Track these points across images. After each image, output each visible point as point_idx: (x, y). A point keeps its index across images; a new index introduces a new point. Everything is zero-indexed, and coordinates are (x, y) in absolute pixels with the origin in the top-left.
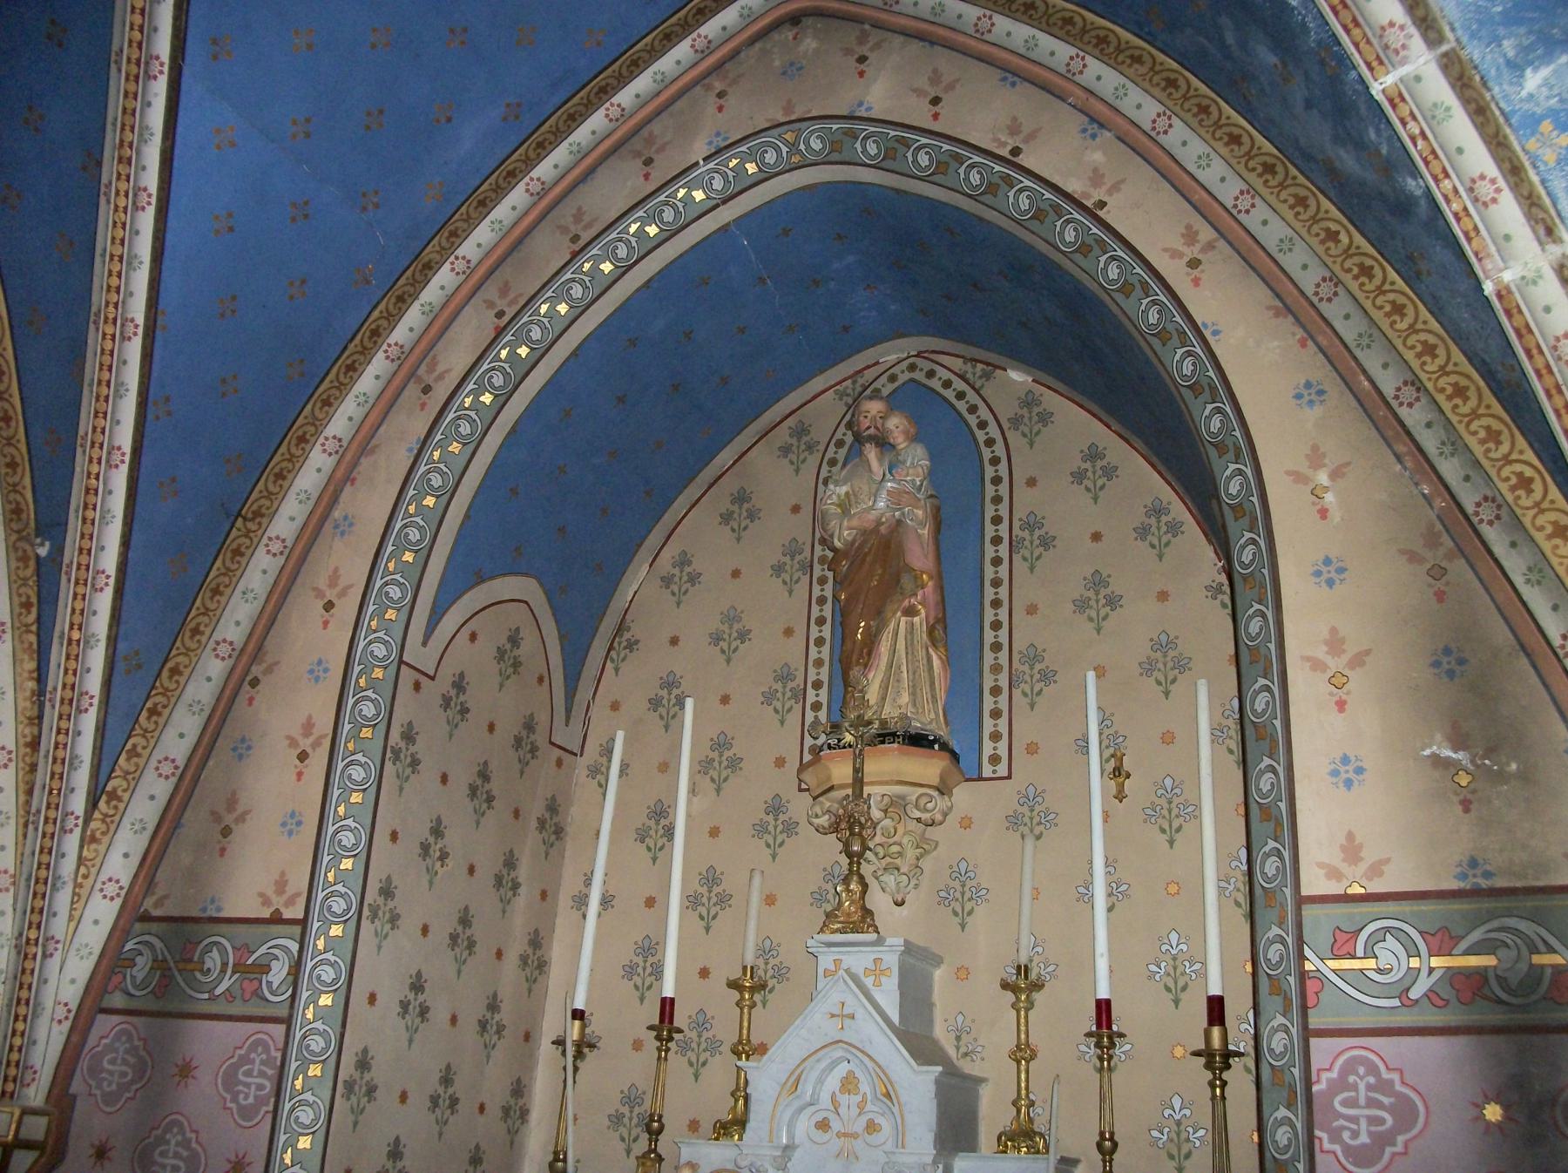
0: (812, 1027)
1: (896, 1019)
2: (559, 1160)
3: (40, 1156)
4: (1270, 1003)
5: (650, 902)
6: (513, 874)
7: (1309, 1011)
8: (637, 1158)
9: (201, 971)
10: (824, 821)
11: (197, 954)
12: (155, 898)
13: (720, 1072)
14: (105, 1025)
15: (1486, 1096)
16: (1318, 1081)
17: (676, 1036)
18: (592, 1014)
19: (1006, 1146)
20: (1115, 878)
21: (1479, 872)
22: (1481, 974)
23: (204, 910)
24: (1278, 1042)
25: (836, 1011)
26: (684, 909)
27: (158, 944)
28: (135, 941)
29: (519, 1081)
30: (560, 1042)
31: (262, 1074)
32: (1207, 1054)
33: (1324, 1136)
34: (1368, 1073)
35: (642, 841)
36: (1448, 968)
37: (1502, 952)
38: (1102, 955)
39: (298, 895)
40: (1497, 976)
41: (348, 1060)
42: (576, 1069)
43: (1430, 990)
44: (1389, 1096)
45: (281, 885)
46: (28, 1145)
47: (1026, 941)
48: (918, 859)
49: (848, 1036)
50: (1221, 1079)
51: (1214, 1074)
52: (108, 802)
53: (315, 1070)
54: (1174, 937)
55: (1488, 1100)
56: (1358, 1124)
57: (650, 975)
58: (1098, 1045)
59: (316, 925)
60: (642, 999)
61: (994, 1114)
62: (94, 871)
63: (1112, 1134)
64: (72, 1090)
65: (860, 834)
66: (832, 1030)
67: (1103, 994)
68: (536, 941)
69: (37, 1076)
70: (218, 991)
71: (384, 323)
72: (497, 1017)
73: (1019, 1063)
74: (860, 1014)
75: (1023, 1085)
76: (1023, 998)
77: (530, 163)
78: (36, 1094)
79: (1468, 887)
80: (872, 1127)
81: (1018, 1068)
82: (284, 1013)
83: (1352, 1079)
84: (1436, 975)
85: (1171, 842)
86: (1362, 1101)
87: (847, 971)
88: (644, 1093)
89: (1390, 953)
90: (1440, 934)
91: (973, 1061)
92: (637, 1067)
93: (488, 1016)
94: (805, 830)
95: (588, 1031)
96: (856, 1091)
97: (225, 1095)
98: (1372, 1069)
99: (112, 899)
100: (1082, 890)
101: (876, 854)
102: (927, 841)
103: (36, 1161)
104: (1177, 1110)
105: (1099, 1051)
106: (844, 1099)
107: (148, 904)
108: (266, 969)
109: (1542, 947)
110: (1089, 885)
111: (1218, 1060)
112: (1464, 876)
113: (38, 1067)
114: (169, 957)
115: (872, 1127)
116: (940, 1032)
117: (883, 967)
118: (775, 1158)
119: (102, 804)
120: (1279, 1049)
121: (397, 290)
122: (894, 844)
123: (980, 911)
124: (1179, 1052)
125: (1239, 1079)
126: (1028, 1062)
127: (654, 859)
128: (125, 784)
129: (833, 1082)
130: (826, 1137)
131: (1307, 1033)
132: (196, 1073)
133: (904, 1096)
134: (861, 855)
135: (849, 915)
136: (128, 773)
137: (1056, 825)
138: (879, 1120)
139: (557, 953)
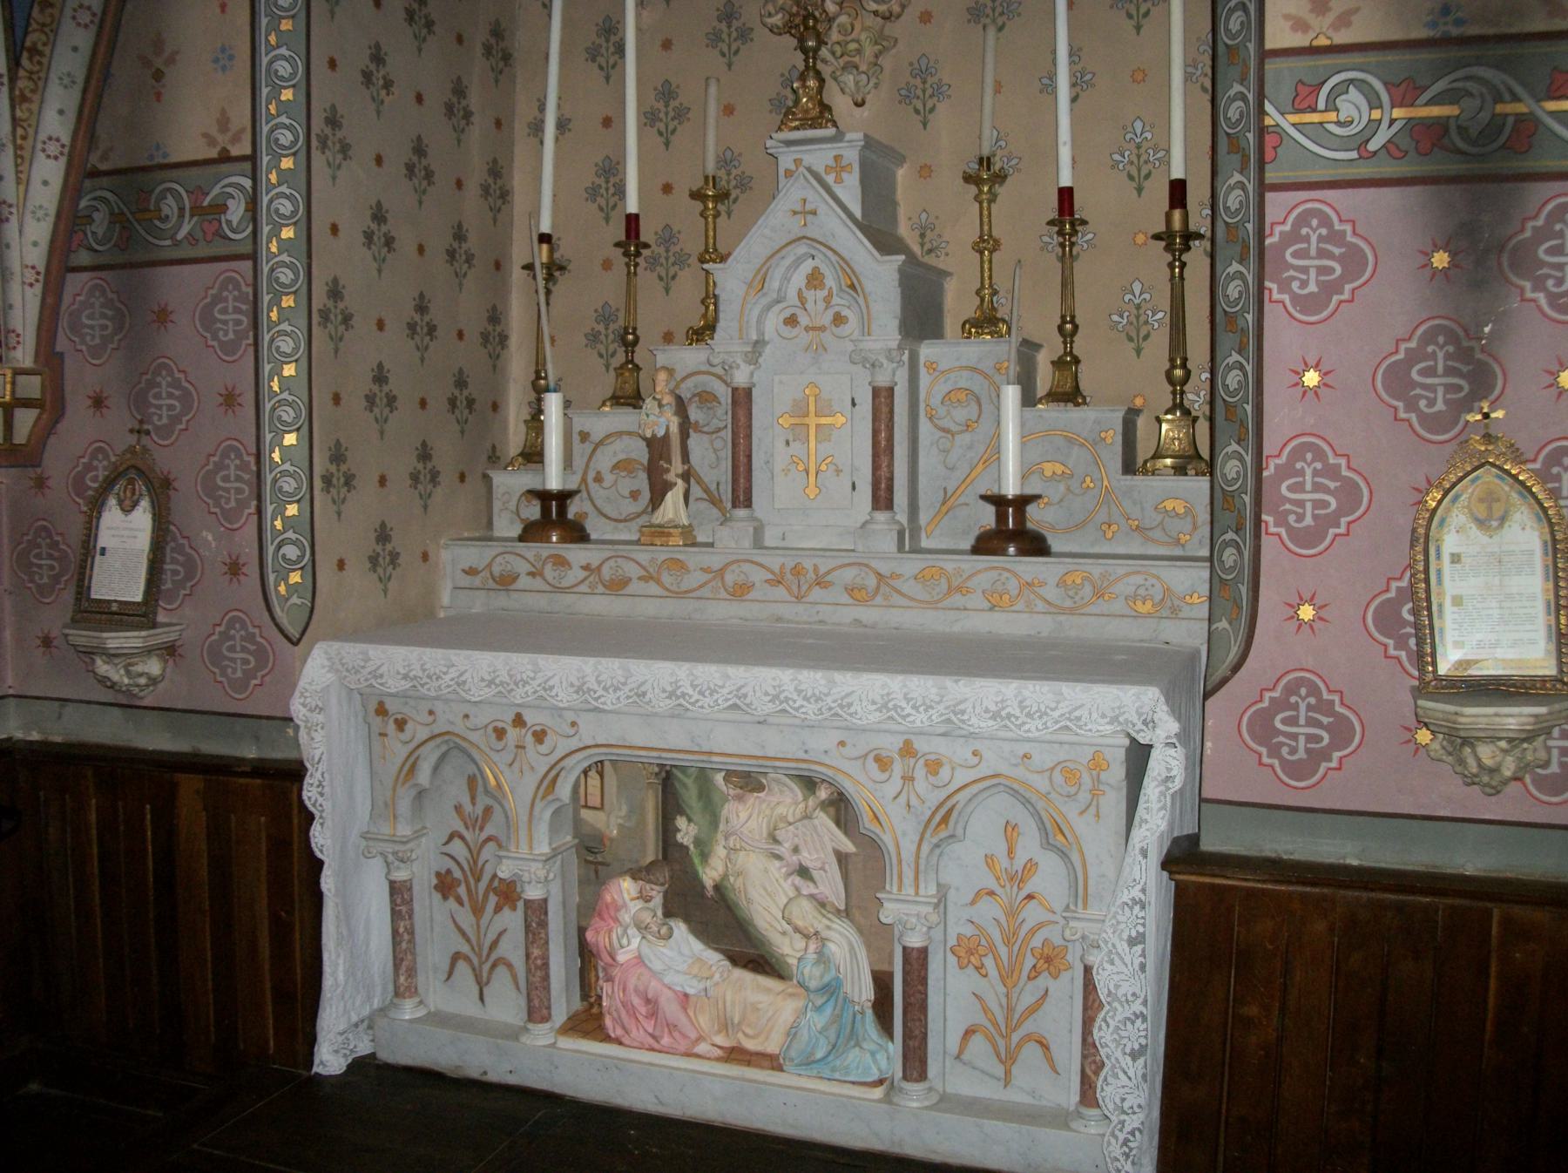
0: (776, 222)
1: (858, 214)
2: (541, 378)
3: (40, 414)
4: (1227, 160)
5: (607, 122)
6: (464, 103)
7: (1267, 167)
8: (615, 369)
9: (160, 219)
10: (777, 20)
11: (153, 201)
12: (99, 153)
13: (688, 284)
14: (76, 284)
15: (1435, 245)
16: (1271, 234)
17: (645, 252)
18: (559, 239)
19: (970, 333)
20: (1079, 67)
21: (1450, 18)
22: (1441, 125)
23: (151, 157)
24: (1233, 200)
25: (798, 208)
26: (641, 127)
27: (108, 195)
28: (88, 197)
29: (494, 308)
30: (529, 267)
31: (237, 310)
32: (1165, 237)
33: (1274, 286)
34: (1320, 225)
35: (594, 60)
36: (1410, 119)
37: (1466, 102)
38: (1065, 143)
39: (243, 130)
40: (1459, 127)
41: (320, 298)
42: (548, 292)
43: (1389, 141)
44: (1340, 247)
45: (224, 123)
46: (27, 403)
47: (988, 134)
48: (877, 57)
49: (811, 232)
50: (1180, 260)
51: (1174, 256)
52: (30, 59)
53: (288, 302)
54: (1138, 126)
55: (1436, 248)
56: (1297, 741)
57: (613, 195)
58: (1061, 233)
59: (265, 159)
60: (607, 219)
61: (958, 302)
62: (31, 131)
63: (1073, 317)
64: (58, 349)
65: (814, 27)
66: (795, 226)
67: (1066, 181)
68: (495, 171)
69: (21, 339)
70: (180, 236)
72: (464, 246)
73: (981, 253)
74: (822, 209)
75: (986, 275)
76: (986, 189)
78: (24, 355)
79: (1438, 35)
80: (839, 320)
81: (982, 258)
82: (248, 249)
83: (1293, 699)
85: (1138, 28)
86: (1313, 252)
87: (809, 170)
88: (618, 310)
89: (1352, 106)
90: (1404, 86)
91: (937, 256)
92: (609, 288)
93: (456, 245)
94: (761, 34)
95: (557, 255)
96: (821, 285)
97: (206, 334)
98: (1325, 221)
100: (1045, 81)
101: (833, 53)
102: (886, 38)
103: (38, 418)
104: (1137, 295)
105: (1061, 240)
106: (810, 295)
107: (94, 160)
108: (223, 208)
109: (1507, 96)
110: (1052, 76)
111: (1177, 241)
112: (1433, 25)
113: (20, 331)
114: (125, 210)
115: (839, 320)
116: (904, 230)
117: (843, 164)
118: (746, 354)
119: (25, 62)
120: (1232, 475)
122: (853, 41)
123: (942, 108)
124: (1141, 238)
125: (1197, 258)
126: (991, 253)
127: (607, 78)
128: (44, 38)
129: (799, 279)
130: (795, 331)
131: (1263, 187)
132: (174, 317)
133: (868, 285)
134: (816, 50)
135: (807, 111)
136: (44, 25)
137: (1019, 15)
138: (845, 312)
139: (518, 182)
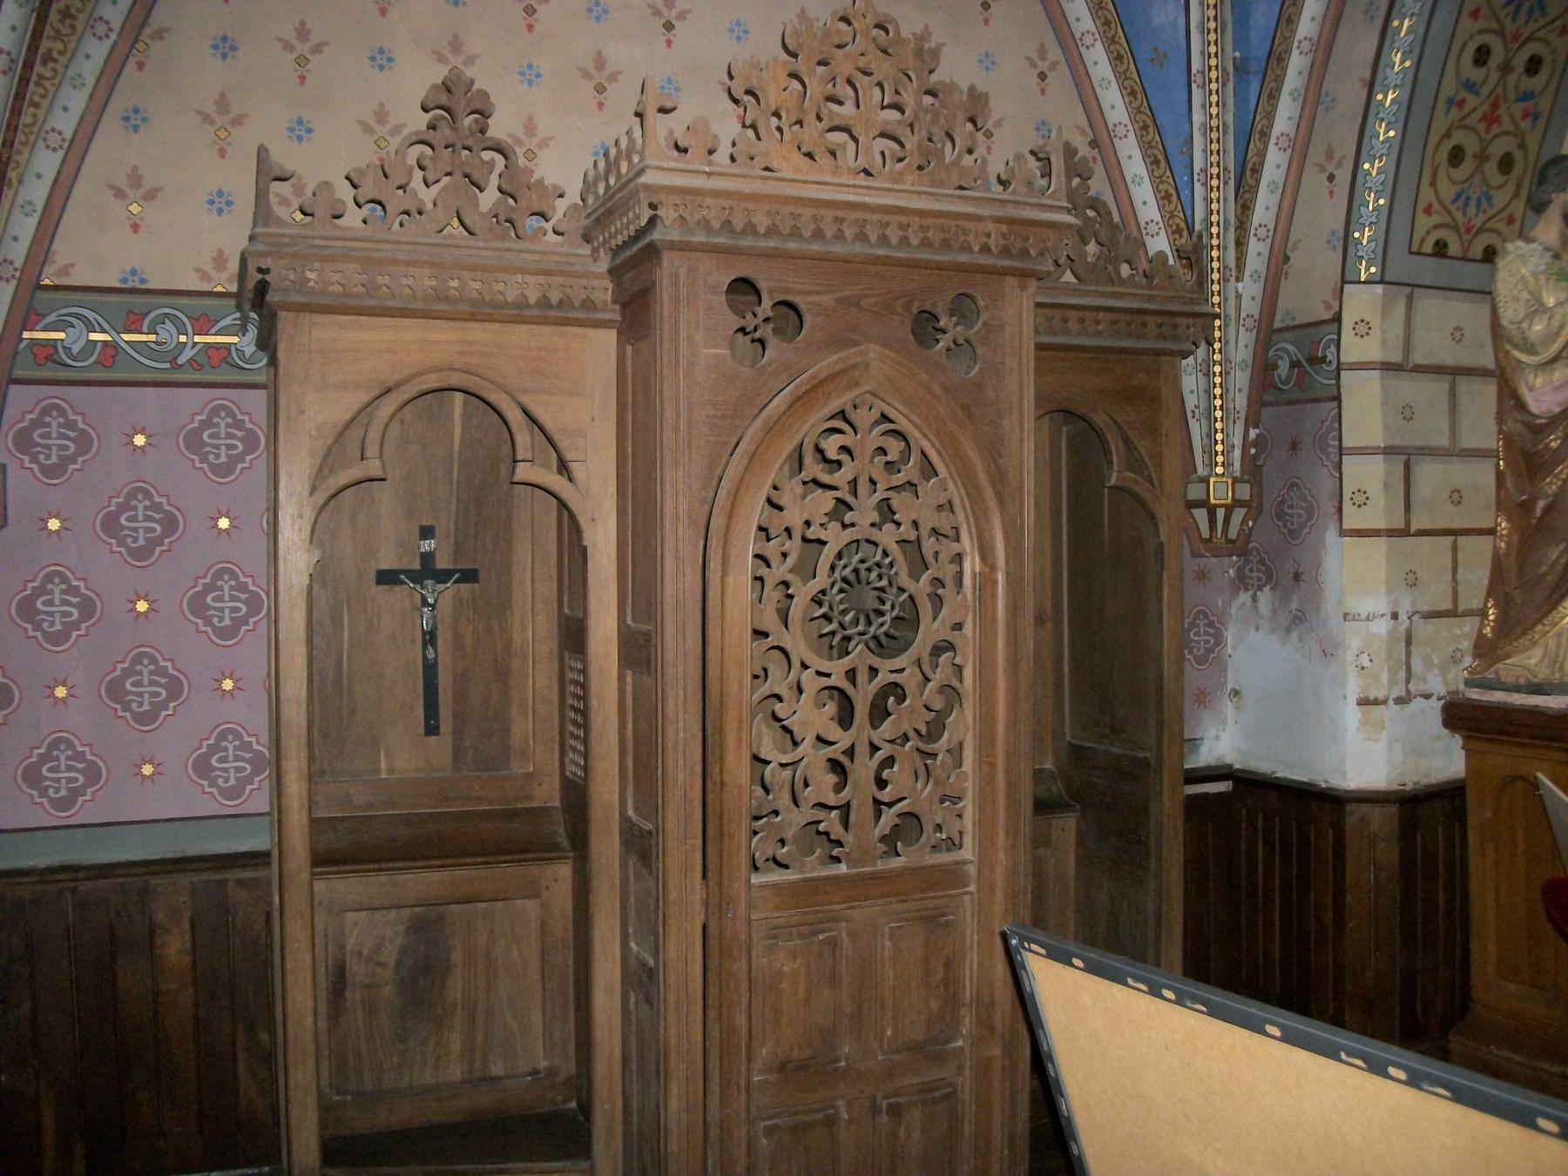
84: (198, 348)
99: (1115, 126)
121: (1115, 24)
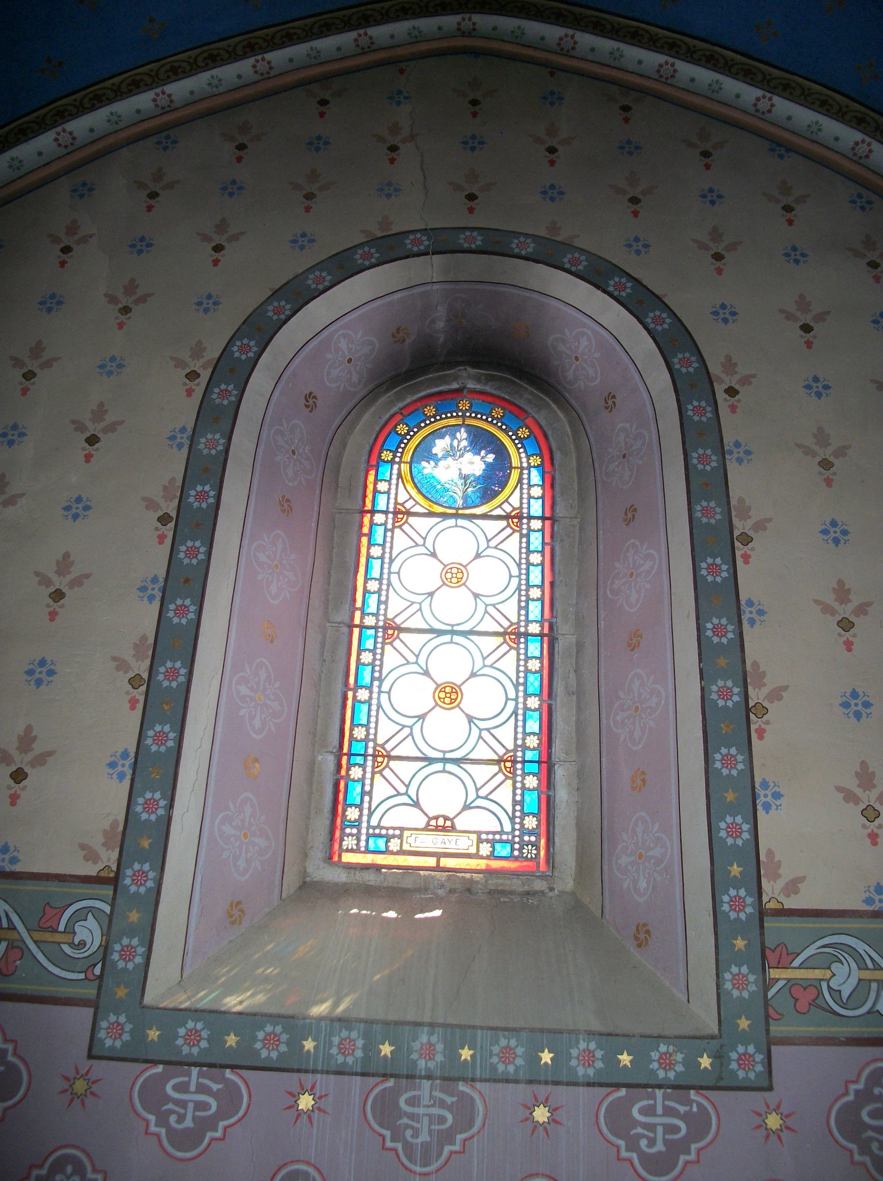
71: (759, 77)
77: (272, 45)
97: (681, 1163)
131: (769, 1043)
